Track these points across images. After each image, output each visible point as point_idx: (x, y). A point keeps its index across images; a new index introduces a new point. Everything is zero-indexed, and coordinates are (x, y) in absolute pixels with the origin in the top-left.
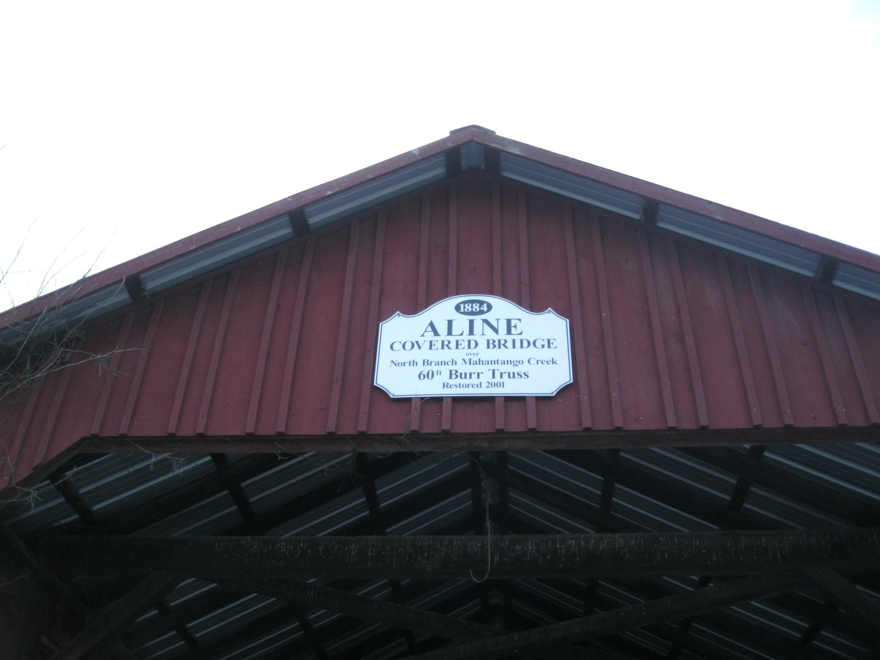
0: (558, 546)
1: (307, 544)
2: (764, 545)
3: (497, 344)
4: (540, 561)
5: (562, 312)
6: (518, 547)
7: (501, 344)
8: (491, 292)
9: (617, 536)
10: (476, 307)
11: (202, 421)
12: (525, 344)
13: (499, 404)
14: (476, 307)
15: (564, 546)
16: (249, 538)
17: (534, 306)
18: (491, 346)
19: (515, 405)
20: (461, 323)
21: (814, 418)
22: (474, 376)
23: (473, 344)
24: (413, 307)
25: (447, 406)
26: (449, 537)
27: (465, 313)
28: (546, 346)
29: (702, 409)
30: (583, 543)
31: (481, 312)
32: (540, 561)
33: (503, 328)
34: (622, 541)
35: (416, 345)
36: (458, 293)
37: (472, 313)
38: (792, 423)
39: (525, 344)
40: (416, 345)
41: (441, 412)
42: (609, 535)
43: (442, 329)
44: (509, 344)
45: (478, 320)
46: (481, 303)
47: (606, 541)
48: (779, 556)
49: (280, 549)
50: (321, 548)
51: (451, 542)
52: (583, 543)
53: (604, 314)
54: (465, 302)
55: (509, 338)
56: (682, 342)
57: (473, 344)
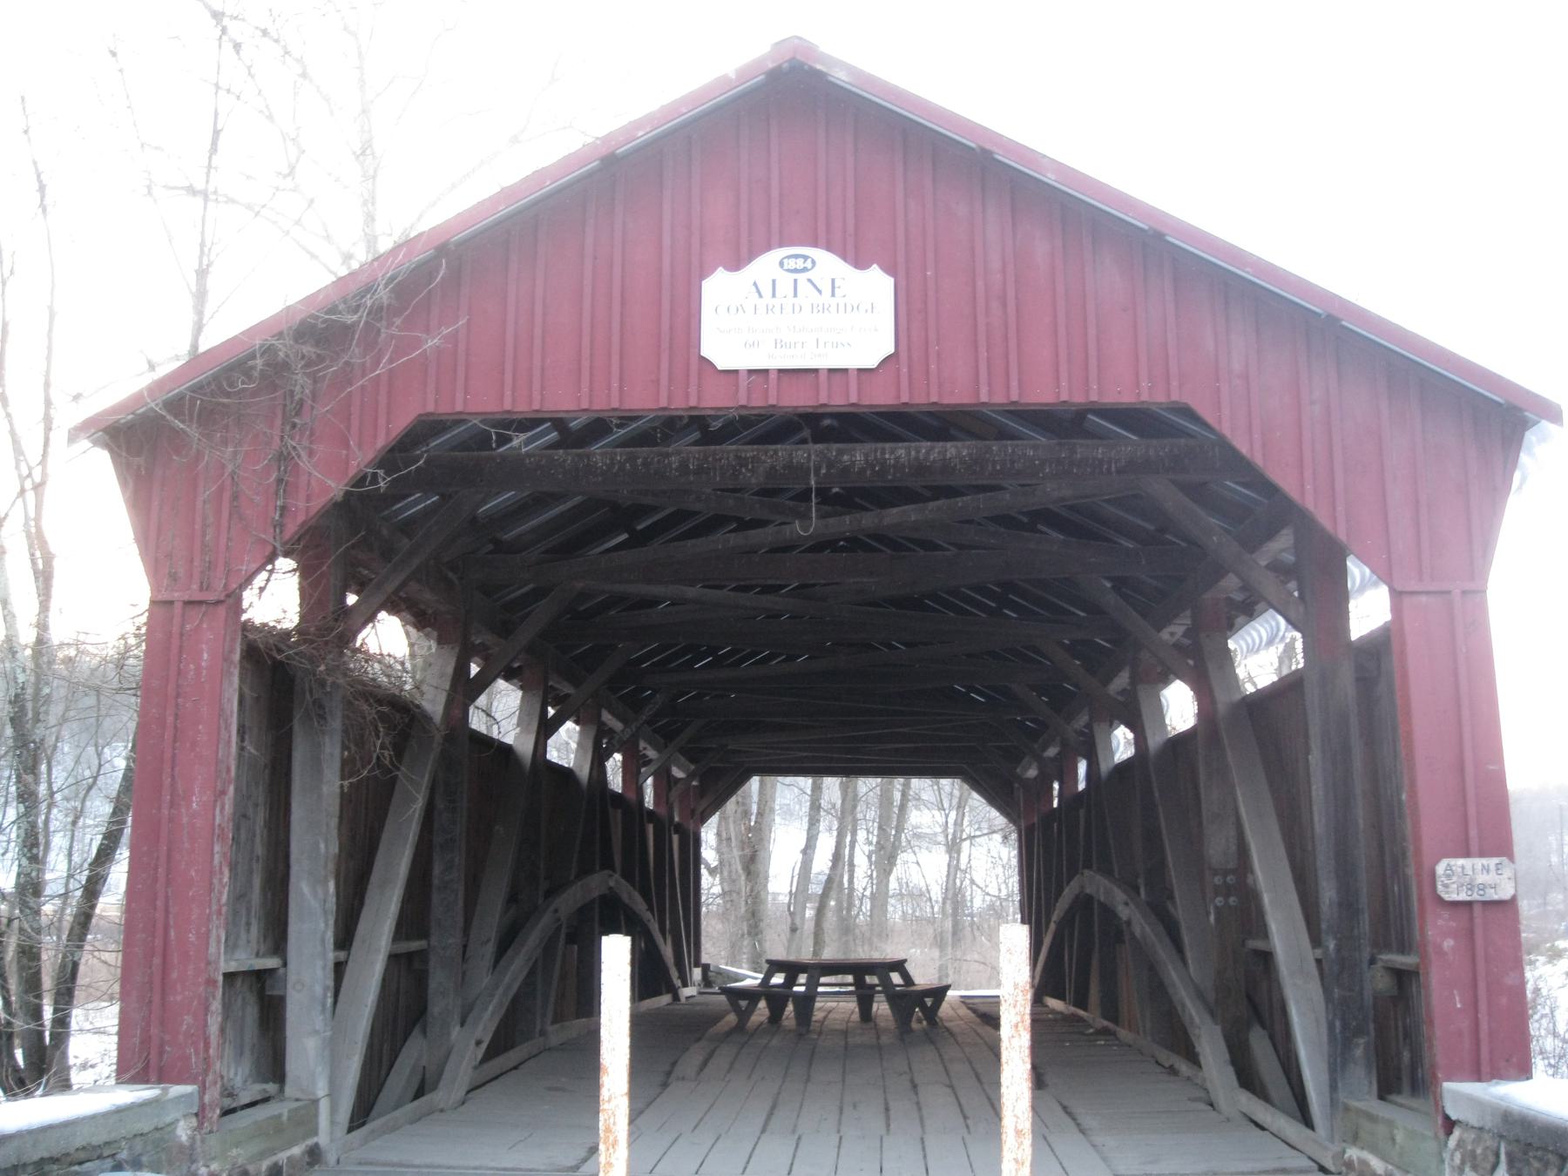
0: (887, 456)
1: (624, 457)
2: (1100, 456)
3: (820, 308)
4: (868, 472)
5: (890, 269)
6: (846, 458)
7: (825, 309)
8: (815, 244)
9: (949, 444)
10: (800, 264)
11: (537, 396)
12: (849, 309)
13: (823, 378)
14: (800, 264)
15: (893, 457)
16: (561, 451)
17: (860, 263)
18: (815, 310)
19: (838, 376)
20: (785, 282)
21: (1119, 392)
22: (799, 346)
23: (797, 309)
24: (736, 264)
25: (773, 376)
26: (773, 447)
27: (788, 270)
28: (870, 310)
29: (1014, 384)
30: (913, 453)
31: (805, 270)
32: (868, 472)
33: (827, 289)
34: (953, 451)
35: (740, 309)
36: (781, 245)
37: (796, 271)
38: (1096, 400)
39: (849, 309)
40: (740, 309)
41: (767, 384)
42: (941, 444)
43: (766, 290)
44: (833, 309)
45: (802, 277)
46: (805, 258)
47: (937, 450)
48: (1113, 469)
49: (596, 463)
50: (639, 461)
51: (776, 452)
52: (913, 453)
53: (929, 273)
54: (789, 257)
55: (833, 301)
56: (1004, 305)
57: (797, 309)
